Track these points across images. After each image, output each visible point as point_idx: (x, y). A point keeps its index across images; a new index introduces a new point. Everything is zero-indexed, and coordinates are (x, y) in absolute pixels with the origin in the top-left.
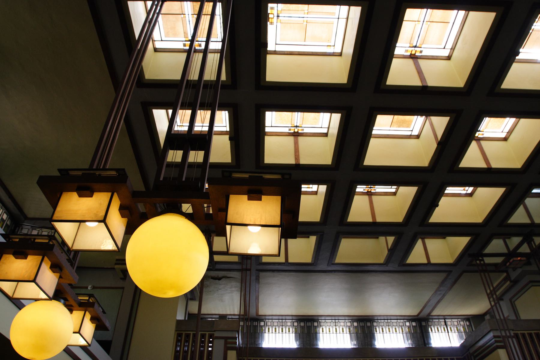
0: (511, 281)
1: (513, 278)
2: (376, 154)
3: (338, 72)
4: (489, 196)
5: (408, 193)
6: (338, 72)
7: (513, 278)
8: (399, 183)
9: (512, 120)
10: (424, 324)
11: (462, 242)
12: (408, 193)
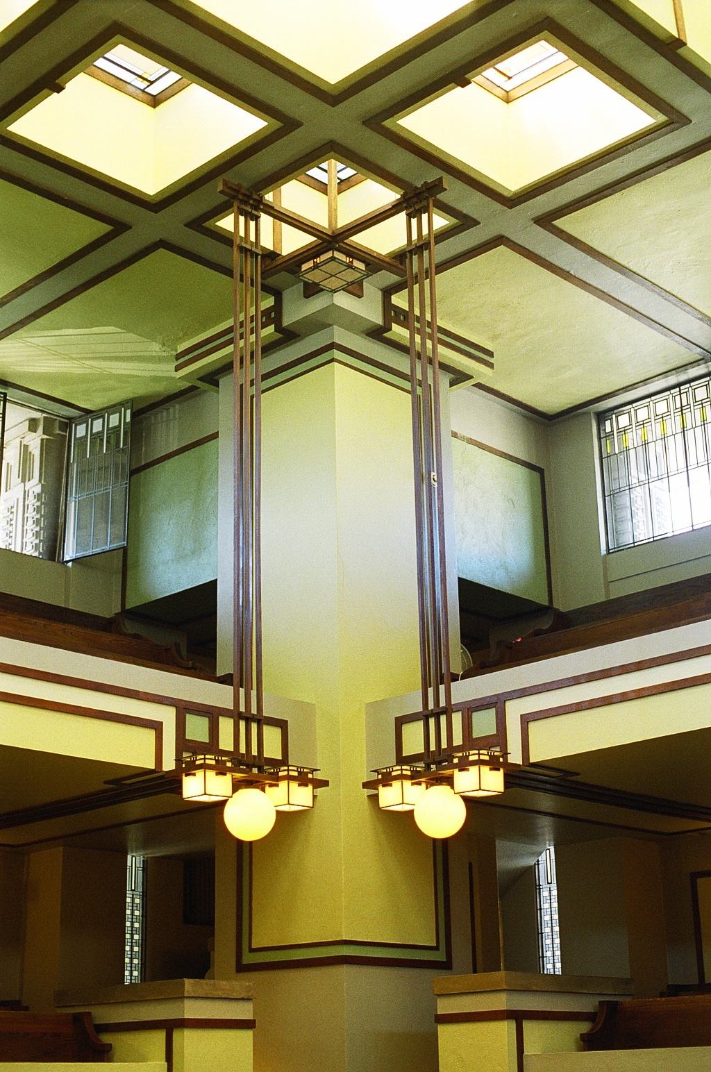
0: (279, 329)
1: (287, 321)
7: (287, 321)
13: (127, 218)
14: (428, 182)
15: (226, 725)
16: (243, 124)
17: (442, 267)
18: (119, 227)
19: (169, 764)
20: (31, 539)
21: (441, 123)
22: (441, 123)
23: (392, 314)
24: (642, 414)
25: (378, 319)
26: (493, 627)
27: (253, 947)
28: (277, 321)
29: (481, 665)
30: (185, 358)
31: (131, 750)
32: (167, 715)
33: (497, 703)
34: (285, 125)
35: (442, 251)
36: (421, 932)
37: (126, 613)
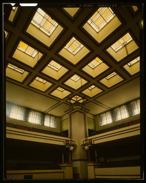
1: (74, 108)
2: (47, 71)
3: (48, 42)
4: (67, 93)
5: (49, 84)
6: (48, 42)
7: (74, 108)
8: (47, 81)
9: (83, 85)
10: (45, 115)
11: (75, 102)
12: (49, 84)
13: (93, 100)
14: (84, 97)
15: (69, 141)
16: (69, 93)
17: (86, 104)
18: (60, 102)
19: (65, 145)
20: (53, 126)
21: (104, 81)
22: (104, 81)
23: (82, 108)
24: (103, 115)
25: (81, 108)
26: (91, 133)
27: (73, 159)
28: (73, 108)
29: (90, 136)
30: (65, 112)
31: (62, 144)
32: (65, 141)
33: (91, 139)
34: (72, 93)
35: (86, 102)
36: (86, 158)
37: (61, 132)
